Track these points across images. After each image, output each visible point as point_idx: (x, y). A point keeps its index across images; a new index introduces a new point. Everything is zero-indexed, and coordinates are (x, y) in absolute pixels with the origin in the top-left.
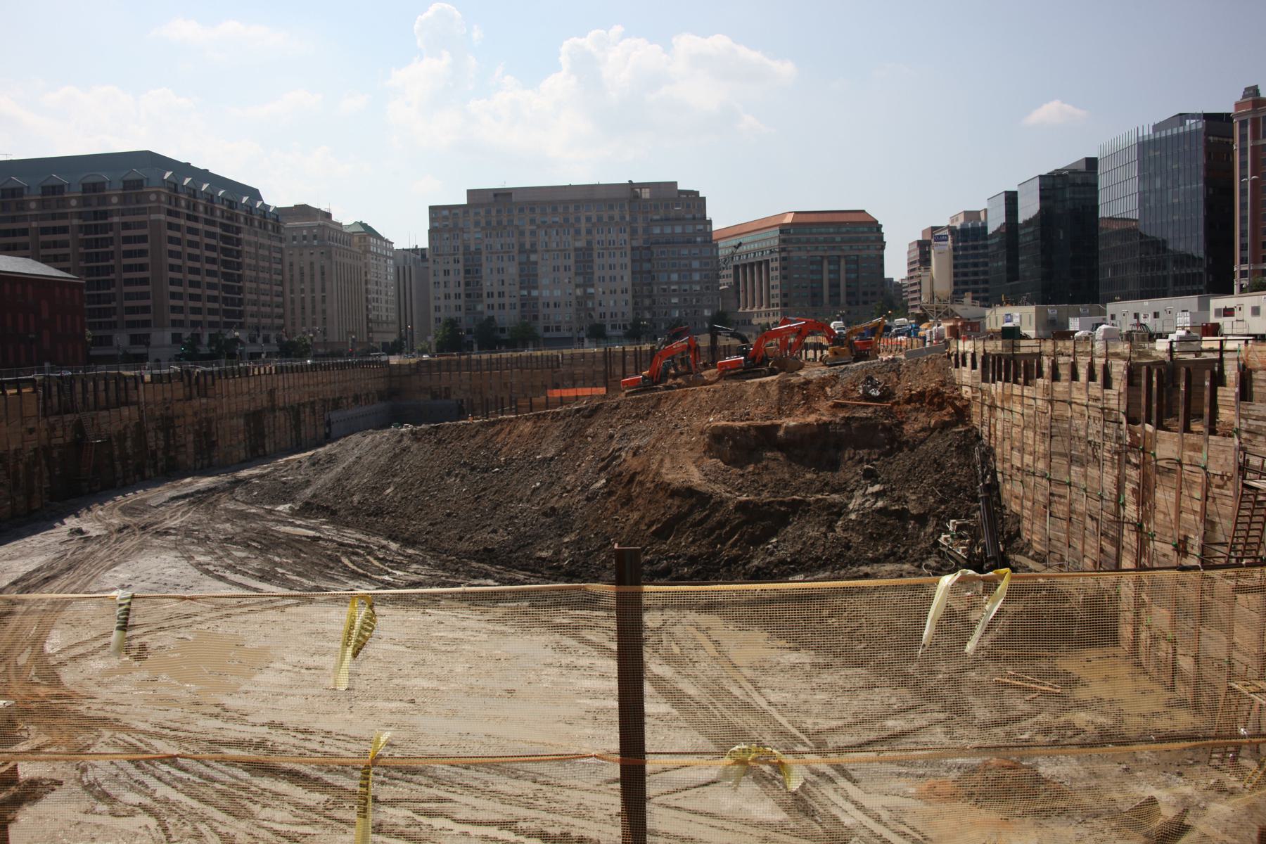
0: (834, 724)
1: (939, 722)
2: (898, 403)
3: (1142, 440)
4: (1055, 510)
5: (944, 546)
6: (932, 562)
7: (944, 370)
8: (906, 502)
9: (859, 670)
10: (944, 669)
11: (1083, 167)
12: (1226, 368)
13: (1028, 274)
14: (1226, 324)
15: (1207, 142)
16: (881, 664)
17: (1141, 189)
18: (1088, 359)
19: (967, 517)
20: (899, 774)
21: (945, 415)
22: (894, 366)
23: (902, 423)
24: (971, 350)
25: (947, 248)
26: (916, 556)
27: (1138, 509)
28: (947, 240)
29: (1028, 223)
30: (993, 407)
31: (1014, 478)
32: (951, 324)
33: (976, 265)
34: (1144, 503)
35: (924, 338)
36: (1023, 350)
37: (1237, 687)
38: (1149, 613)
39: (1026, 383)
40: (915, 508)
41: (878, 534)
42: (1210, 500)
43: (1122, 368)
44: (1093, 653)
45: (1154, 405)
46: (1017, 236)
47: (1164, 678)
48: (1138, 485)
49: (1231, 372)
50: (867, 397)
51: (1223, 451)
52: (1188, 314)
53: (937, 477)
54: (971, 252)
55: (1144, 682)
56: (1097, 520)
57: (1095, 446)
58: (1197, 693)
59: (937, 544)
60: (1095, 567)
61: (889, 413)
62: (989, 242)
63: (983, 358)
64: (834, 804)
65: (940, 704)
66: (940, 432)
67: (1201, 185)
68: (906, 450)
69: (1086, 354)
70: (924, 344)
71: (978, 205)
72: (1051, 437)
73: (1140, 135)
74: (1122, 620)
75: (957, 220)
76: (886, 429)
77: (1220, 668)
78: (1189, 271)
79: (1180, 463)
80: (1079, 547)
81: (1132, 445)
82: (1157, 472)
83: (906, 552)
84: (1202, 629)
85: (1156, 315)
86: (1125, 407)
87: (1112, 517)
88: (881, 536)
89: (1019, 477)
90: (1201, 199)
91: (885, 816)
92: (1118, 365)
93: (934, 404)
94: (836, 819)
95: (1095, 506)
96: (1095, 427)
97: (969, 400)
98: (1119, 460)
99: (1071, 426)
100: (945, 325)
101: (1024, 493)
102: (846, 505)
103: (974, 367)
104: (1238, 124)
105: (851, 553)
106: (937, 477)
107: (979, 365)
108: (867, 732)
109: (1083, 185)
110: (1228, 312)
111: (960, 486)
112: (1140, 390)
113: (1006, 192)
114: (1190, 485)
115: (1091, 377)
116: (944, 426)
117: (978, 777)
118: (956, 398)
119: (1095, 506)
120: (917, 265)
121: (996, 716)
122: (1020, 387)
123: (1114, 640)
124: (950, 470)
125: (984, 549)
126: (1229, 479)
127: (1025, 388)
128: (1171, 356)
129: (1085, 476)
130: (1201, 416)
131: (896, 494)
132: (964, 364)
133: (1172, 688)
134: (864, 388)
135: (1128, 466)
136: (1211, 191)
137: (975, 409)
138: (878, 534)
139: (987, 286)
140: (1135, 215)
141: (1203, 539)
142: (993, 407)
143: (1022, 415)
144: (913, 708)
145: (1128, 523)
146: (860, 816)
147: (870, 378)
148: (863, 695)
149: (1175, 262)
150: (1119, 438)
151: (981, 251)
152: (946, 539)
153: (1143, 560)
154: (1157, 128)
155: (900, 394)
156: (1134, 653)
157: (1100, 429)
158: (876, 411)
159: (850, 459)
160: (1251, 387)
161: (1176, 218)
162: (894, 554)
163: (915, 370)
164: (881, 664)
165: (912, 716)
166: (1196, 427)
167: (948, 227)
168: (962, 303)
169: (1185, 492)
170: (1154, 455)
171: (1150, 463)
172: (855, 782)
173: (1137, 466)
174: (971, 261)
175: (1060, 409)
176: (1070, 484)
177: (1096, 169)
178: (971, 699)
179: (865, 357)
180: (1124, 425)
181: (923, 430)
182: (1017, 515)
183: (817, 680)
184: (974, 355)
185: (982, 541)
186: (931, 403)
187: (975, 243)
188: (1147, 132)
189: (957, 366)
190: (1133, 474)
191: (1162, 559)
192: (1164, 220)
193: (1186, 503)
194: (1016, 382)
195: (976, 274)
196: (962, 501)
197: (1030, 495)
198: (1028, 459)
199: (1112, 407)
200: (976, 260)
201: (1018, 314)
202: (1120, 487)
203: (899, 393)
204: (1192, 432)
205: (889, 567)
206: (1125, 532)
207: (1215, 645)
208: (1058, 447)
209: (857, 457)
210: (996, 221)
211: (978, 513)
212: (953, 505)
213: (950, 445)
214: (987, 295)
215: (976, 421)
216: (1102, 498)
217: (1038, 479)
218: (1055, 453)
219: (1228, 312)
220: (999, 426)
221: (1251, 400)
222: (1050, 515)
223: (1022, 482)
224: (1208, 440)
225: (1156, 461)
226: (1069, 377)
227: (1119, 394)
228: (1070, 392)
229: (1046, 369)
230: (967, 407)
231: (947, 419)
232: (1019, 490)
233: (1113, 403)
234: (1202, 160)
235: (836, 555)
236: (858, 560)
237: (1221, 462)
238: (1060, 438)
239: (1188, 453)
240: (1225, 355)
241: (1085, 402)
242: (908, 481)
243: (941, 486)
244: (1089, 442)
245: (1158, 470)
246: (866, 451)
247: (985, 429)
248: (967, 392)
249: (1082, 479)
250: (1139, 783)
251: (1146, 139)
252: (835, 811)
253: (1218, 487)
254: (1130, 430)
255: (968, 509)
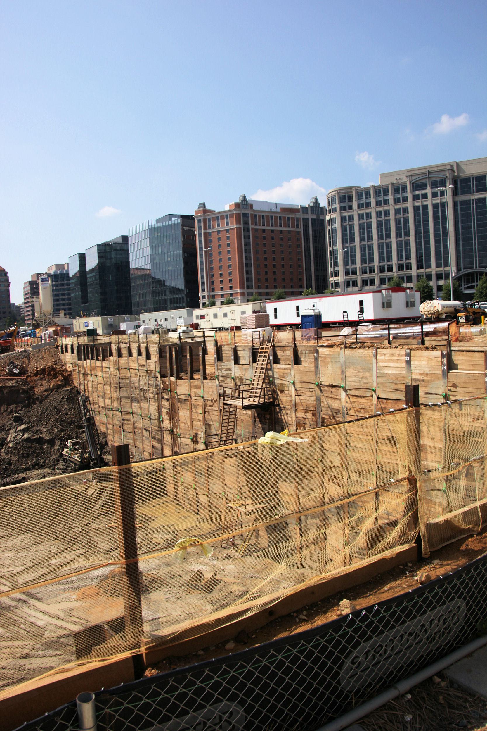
0: (20, 569)
1: (79, 555)
2: (30, 376)
3: (169, 386)
4: (126, 428)
5: (66, 456)
6: (60, 466)
7: (55, 355)
8: (41, 433)
9: (28, 535)
10: (78, 525)
11: (120, 241)
12: (207, 345)
13: (93, 299)
14: (202, 323)
15: (183, 229)
16: (41, 529)
17: (152, 253)
18: (137, 345)
19: (77, 437)
20: (64, 590)
21: (59, 380)
22: (26, 354)
23: (33, 387)
24: (71, 343)
25: (49, 285)
26: (51, 464)
27: (170, 423)
28: (48, 281)
29: (92, 271)
30: (85, 374)
31: (101, 413)
32: (54, 329)
33: (63, 295)
34: (173, 419)
35: (41, 337)
36: (99, 342)
37: (230, 505)
38: (182, 476)
39: (103, 360)
40: (47, 436)
41: (27, 454)
42: (207, 413)
43: (155, 348)
44: (155, 502)
45: (175, 367)
46: (86, 278)
47: (193, 508)
48: (169, 409)
49: (211, 348)
50: (11, 374)
51: (211, 388)
52: (182, 318)
53: (58, 416)
54: (60, 287)
55: (184, 512)
56: (149, 431)
57: (144, 391)
58: (210, 512)
59: (62, 455)
60: (150, 456)
61: (25, 382)
62: (71, 282)
63: (78, 347)
64: (30, 616)
65: (79, 545)
66: (56, 391)
67: (181, 251)
68: (37, 403)
69: (136, 342)
70: (41, 341)
71: (63, 261)
72: (120, 388)
73: (150, 224)
74: (167, 482)
75: (51, 269)
76: (25, 392)
77: (220, 498)
78: (178, 296)
79: (190, 396)
80: (141, 447)
81: (164, 389)
82: (179, 402)
83: (44, 462)
84: (209, 480)
85: (166, 320)
86: (159, 369)
87: (157, 428)
88: (29, 455)
89: (104, 412)
90: (181, 259)
91: (62, 615)
92: (153, 347)
93: (51, 375)
94: (33, 624)
95: (147, 423)
96: (144, 381)
97: (71, 372)
98: (158, 397)
99: (130, 381)
100: (51, 330)
101: (107, 421)
102: (6, 439)
103: (73, 352)
104: (197, 221)
105: (12, 467)
106: (58, 416)
107: (75, 351)
108: (41, 570)
109: (121, 250)
110: (202, 317)
111: (71, 421)
112: (166, 359)
113: (79, 254)
114: (196, 406)
115: (140, 354)
116: (58, 387)
117: (109, 581)
118: (63, 371)
119: (147, 423)
120: (29, 295)
121: (111, 545)
122: (100, 362)
123: (165, 494)
124: (64, 412)
125: (90, 454)
126: (215, 401)
127: (103, 362)
128: (180, 340)
129: (140, 408)
130: (198, 371)
131: (35, 429)
132: (67, 351)
133: (198, 513)
134: (9, 369)
135: (163, 400)
136: (186, 255)
137: (75, 376)
138: (27, 454)
139: (70, 307)
140: (149, 267)
141: (205, 433)
142: (85, 374)
143: (103, 377)
144: (64, 551)
145: (166, 430)
146: (46, 618)
147: (12, 363)
148: (34, 549)
149: (170, 292)
150: (157, 386)
151: (66, 287)
152: (67, 452)
153: (176, 448)
154: (158, 221)
155: (31, 370)
156: (176, 498)
157: (146, 382)
158: (17, 382)
159: (5, 411)
160: (222, 354)
161: (169, 268)
162: (37, 464)
163: (38, 356)
164: (41, 529)
165: (65, 555)
166: (196, 376)
167: (47, 273)
168: (58, 316)
169: (194, 410)
170: (176, 393)
171: (174, 397)
172: (40, 600)
173: (168, 400)
174: (61, 292)
175: (123, 372)
176: (132, 413)
177: (128, 241)
178: (96, 539)
179: (8, 351)
180: (159, 379)
181: (46, 390)
182: (105, 433)
183: (4, 545)
184: (72, 346)
185: (88, 450)
186: (49, 374)
187: (63, 282)
188: (153, 223)
189: (62, 353)
190: (165, 403)
191: (185, 447)
192: (164, 270)
193: (195, 416)
194: (97, 359)
195: (63, 300)
196: (73, 429)
197: (111, 421)
198: (108, 402)
199: (152, 369)
200: (63, 292)
201: (92, 322)
202: (160, 412)
203: (30, 370)
204: (194, 379)
205: (36, 472)
206: (165, 435)
207: (216, 487)
208: (124, 393)
209: (9, 410)
210: (74, 269)
211: (84, 435)
212: (68, 432)
213: (63, 398)
214: (70, 311)
215: (76, 383)
216: (150, 419)
217: (115, 412)
218: (123, 397)
219: (202, 317)
220: (90, 385)
221: (222, 361)
222: (123, 431)
223: (106, 415)
224: (203, 383)
225: (178, 396)
226: (127, 355)
227: (155, 362)
228: (128, 363)
229: (114, 351)
230: (70, 375)
231: (59, 383)
232: (104, 419)
233: (152, 367)
234: (181, 239)
235: (3, 469)
236: (17, 470)
237: (211, 393)
238: (125, 389)
239: (194, 390)
240: (206, 339)
241: (137, 368)
242: (41, 421)
243: (61, 421)
244: (141, 389)
245: (180, 401)
246: (14, 406)
247: (82, 387)
248: (70, 367)
249: (139, 410)
250: (191, 565)
251: (153, 227)
252: (32, 619)
253: (210, 406)
254: (162, 381)
255: (77, 433)
